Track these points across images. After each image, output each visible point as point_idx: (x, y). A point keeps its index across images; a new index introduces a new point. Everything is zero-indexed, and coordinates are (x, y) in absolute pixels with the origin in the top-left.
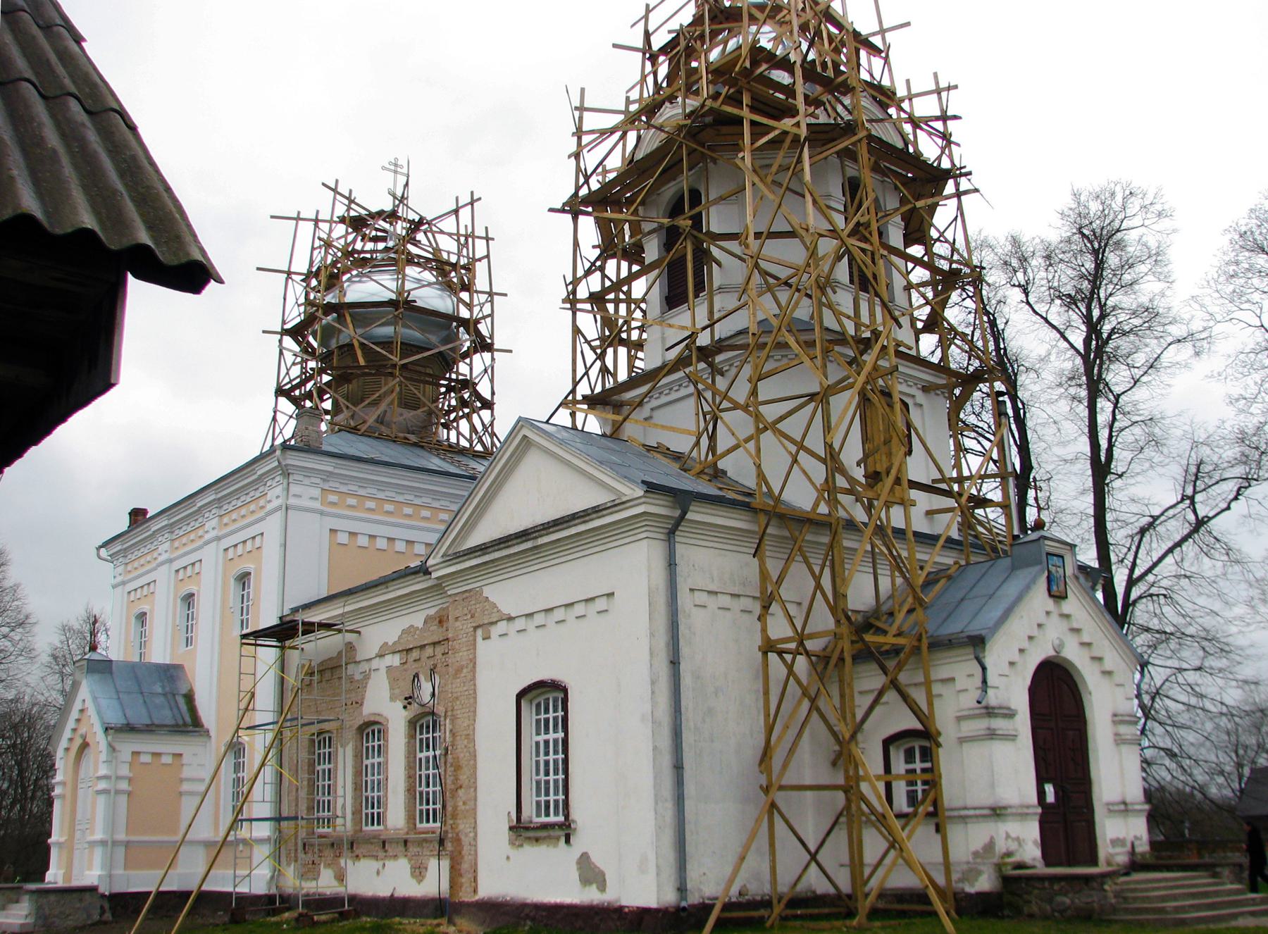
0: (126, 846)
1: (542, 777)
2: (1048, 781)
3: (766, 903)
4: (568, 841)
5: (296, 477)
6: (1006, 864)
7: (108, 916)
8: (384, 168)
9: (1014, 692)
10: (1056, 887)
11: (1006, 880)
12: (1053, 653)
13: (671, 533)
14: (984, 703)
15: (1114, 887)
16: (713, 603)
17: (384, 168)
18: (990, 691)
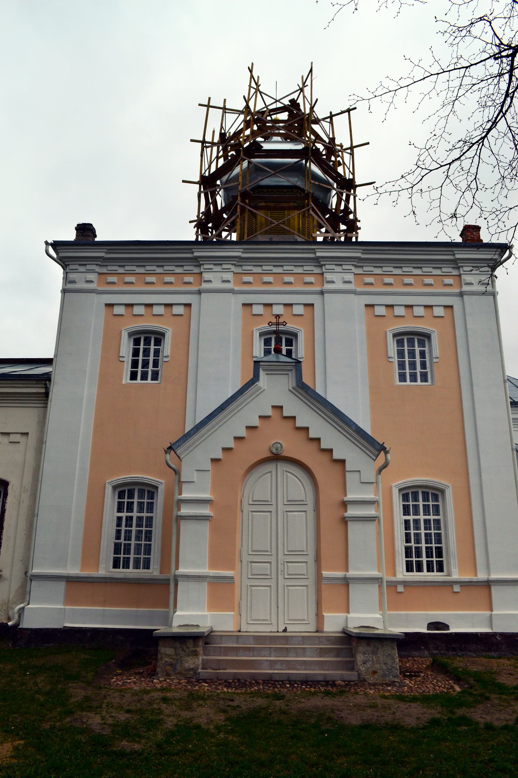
1: (413, 544)
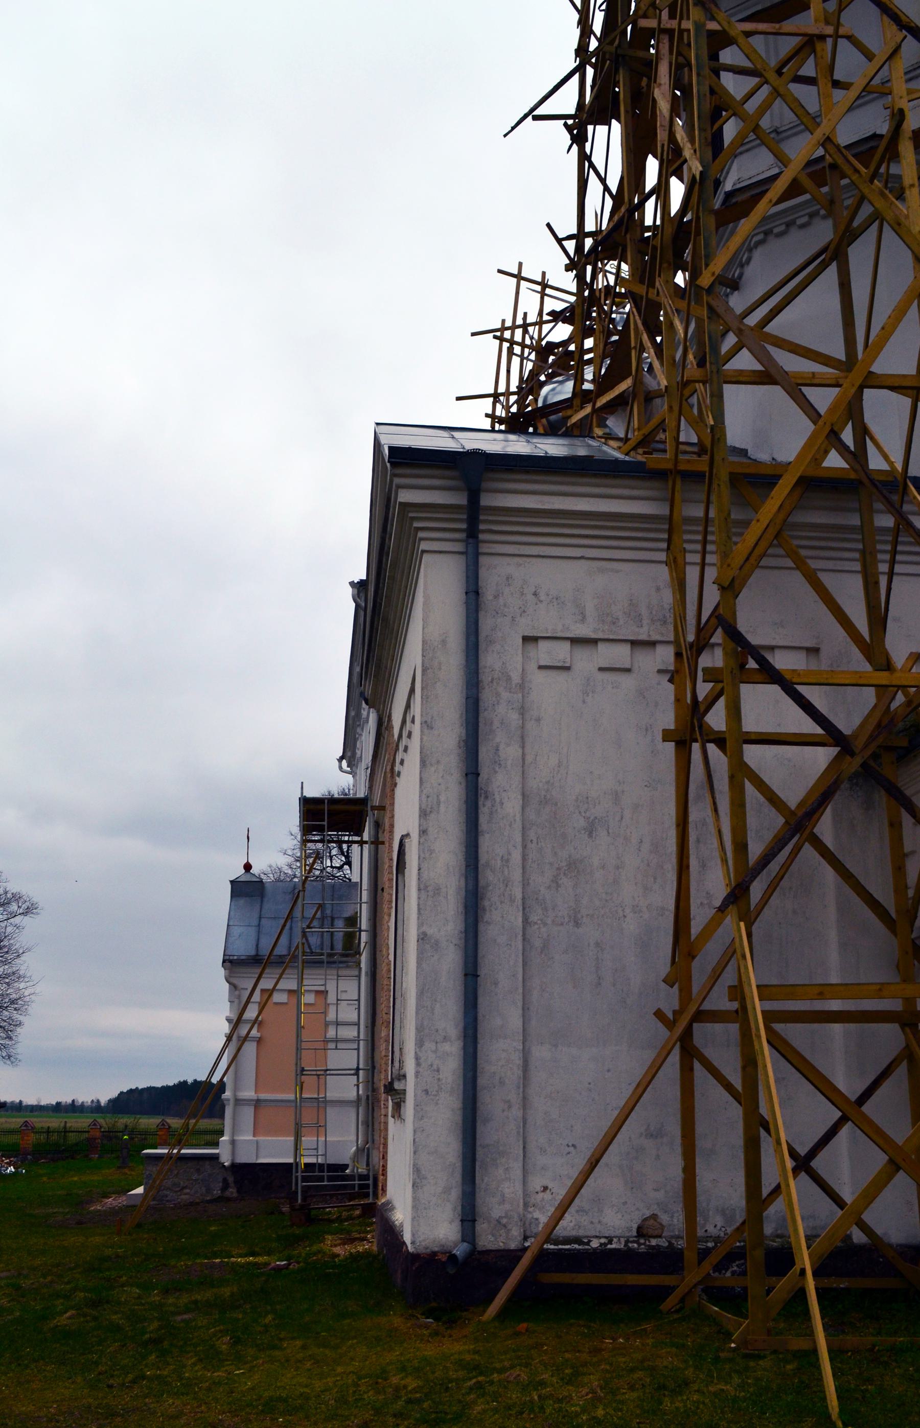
0: (256, 1107)
3: (668, 1260)
7: (232, 1192)
16: (586, 662)
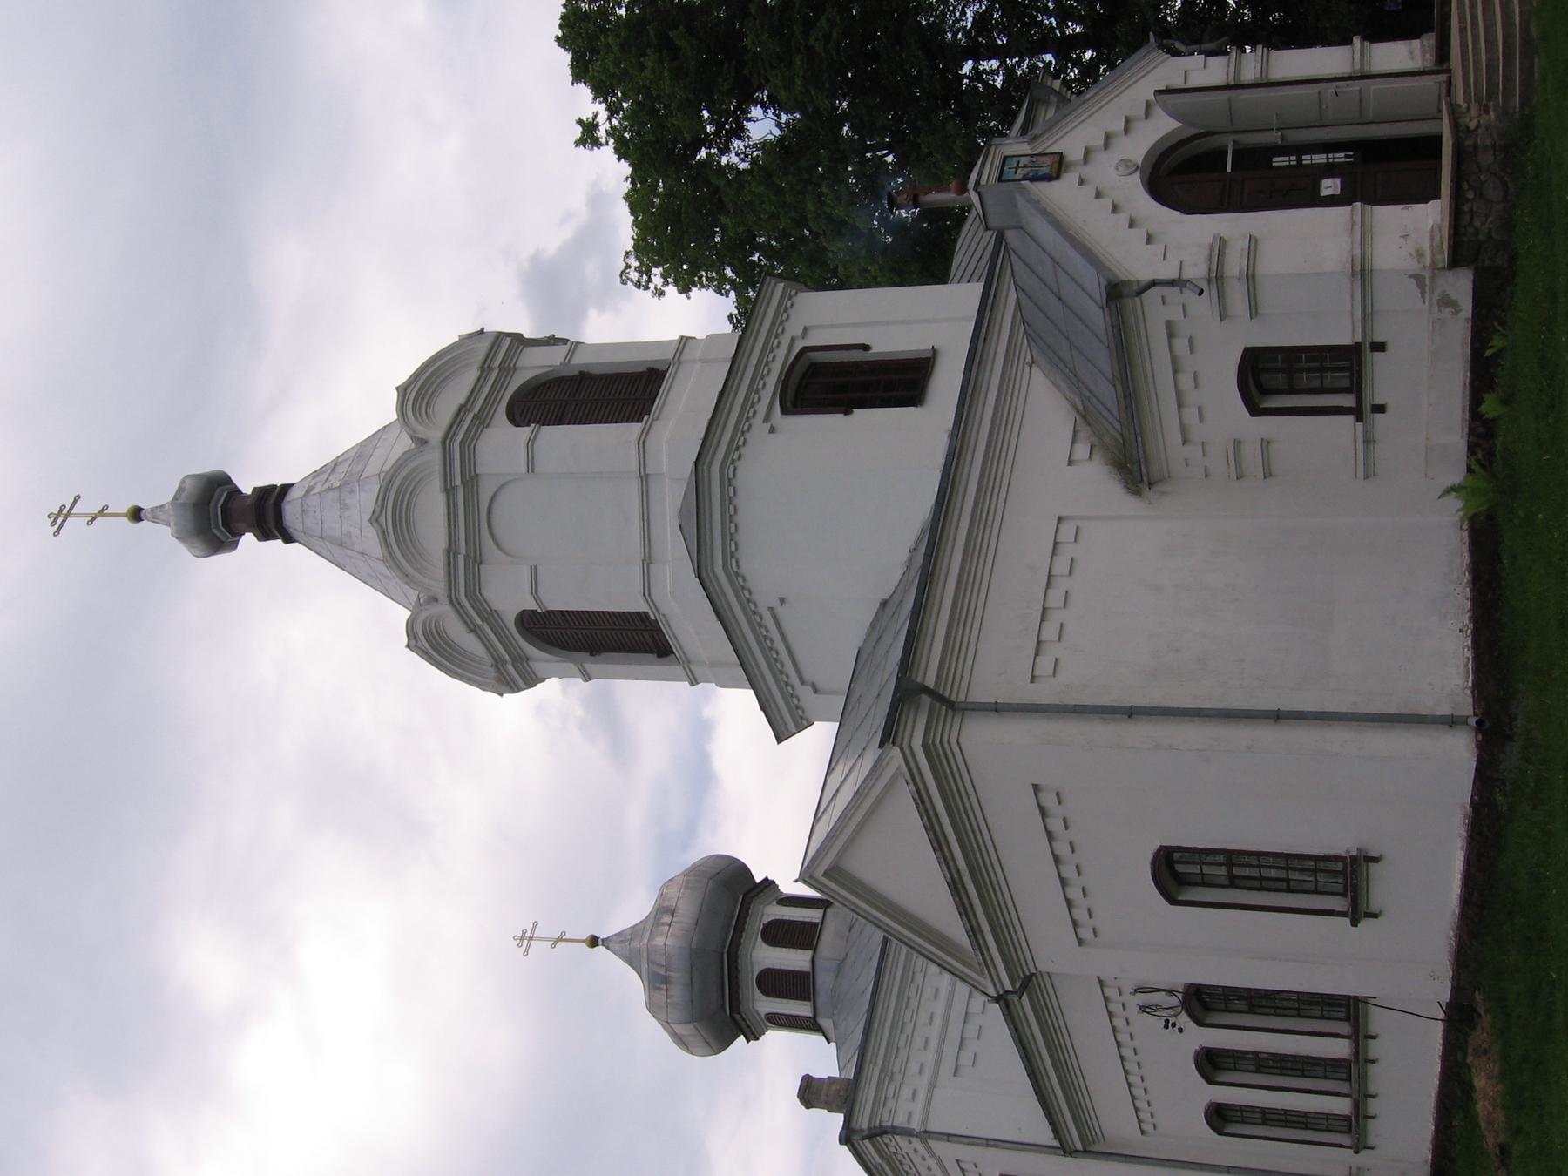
2: (1317, 188)
4: (1376, 860)
5: (885, 1118)
6: (1433, 262)
8: (526, 953)
9: (1190, 237)
10: (1470, 195)
11: (1455, 262)
12: (1137, 175)
13: (951, 705)
14: (1204, 286)
15: (1473, 112)
17: (526, 953)
18: (1186, 275)
